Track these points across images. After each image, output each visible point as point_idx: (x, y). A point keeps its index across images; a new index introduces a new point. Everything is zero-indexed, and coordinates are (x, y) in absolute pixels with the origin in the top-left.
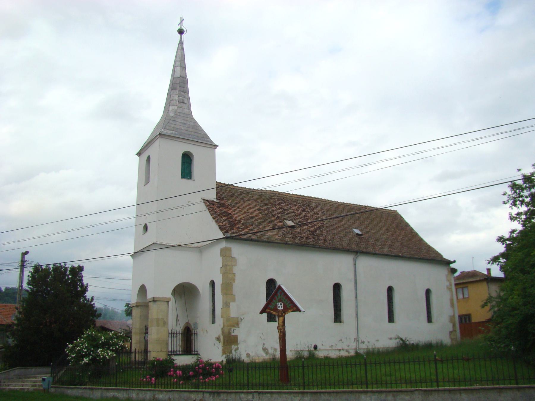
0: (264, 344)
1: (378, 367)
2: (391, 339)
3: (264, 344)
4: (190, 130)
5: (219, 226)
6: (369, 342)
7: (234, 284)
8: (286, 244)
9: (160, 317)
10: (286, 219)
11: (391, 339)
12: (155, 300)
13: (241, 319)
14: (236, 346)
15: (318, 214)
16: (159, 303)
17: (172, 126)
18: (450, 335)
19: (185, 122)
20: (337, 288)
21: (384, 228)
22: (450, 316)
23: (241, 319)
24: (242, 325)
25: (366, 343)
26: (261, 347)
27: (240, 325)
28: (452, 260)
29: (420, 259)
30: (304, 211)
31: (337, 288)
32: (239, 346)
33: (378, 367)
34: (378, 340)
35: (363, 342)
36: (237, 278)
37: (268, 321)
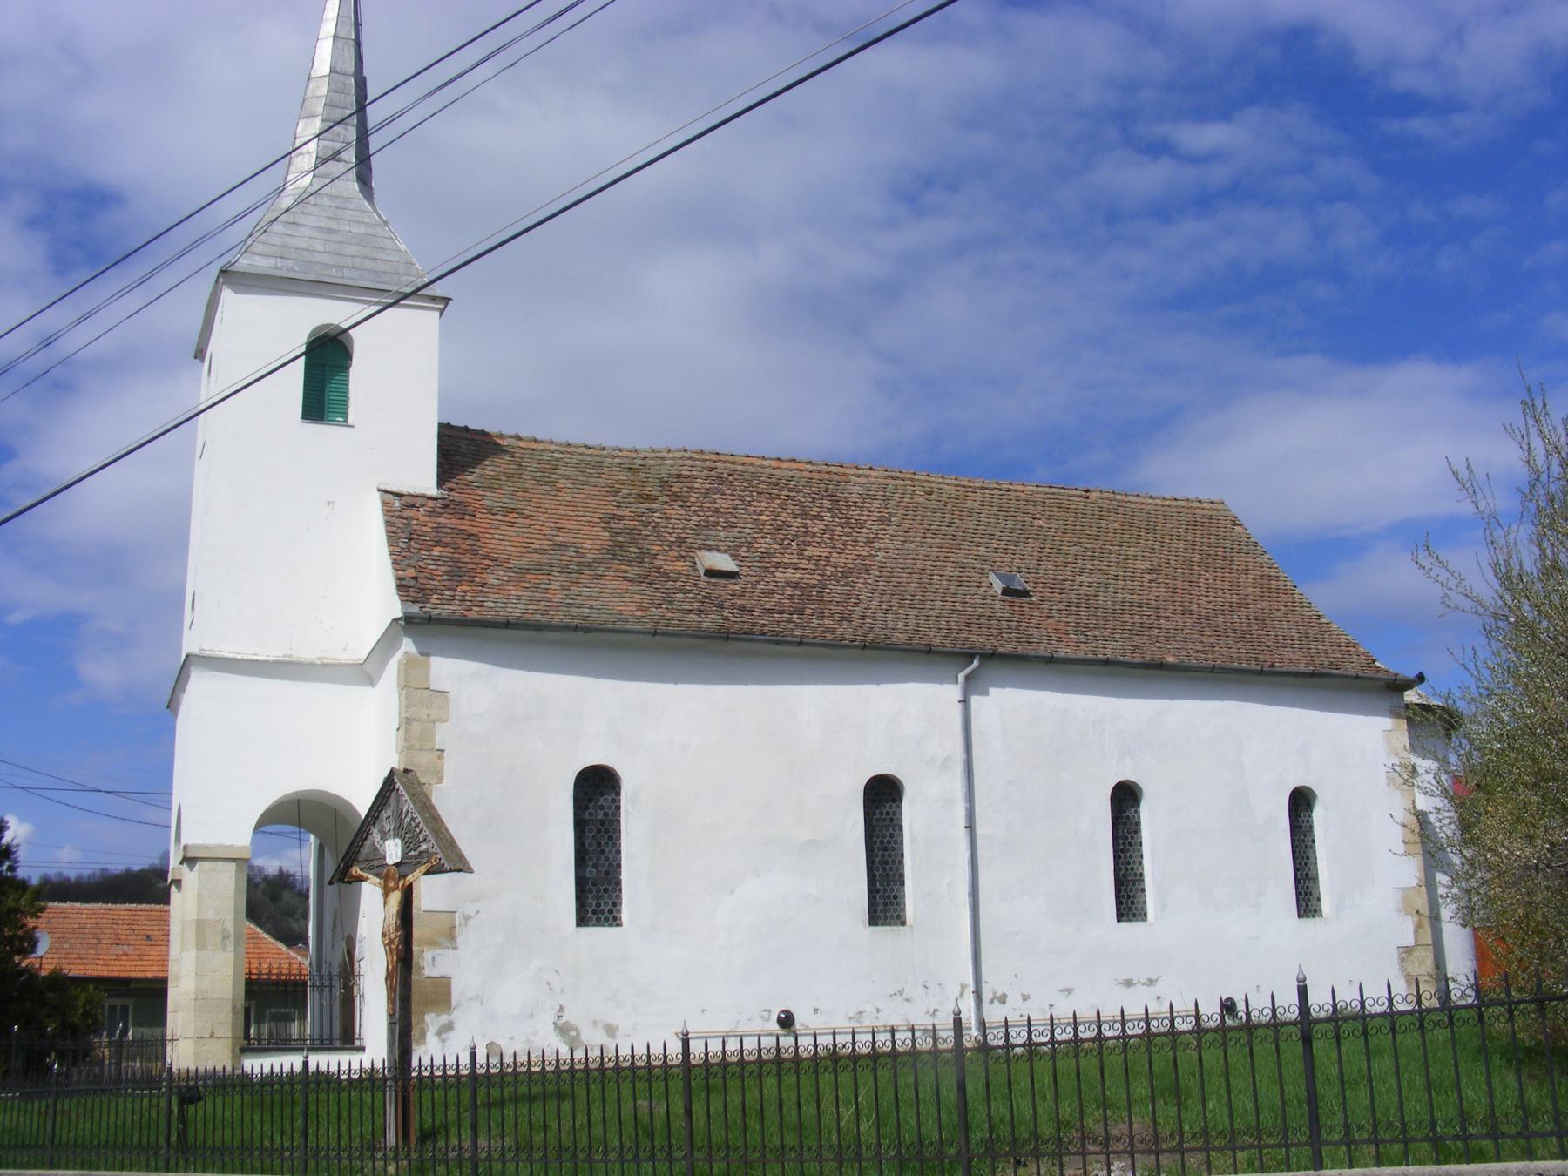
0: (562, 1009)
1: (79, 1141)
2: (1129, 983)
3: (562, 1009)
4: (349, 250)
5: (399, 579)
6: (1025, 998)
7: (435, 787)
8: (929, 652)
9: (210, 915)
10: (709, 548)
11: (1129, 983)
12: (191, 854)
13: (467, 918)
14: (444, 1019)
15: (862, 525)
16: (206, 865)
17: (278, 240)
18: (1402, 960)
19: (333, 225)
20: (882, 796)
21: (1142, 566)
22: (1405, 891)
23: (467, 918)
24: (466, 938)
25: (1014, 999)
26: (550, 1018)
27: (460, 940)
28: (1410, 673)
29: (724, 636)
30: (804, 514)
31: (882, 796)
32: (456, 1016)
33: (79, 1141)
34: (1069, 991)
35: (1003, 999)
36: (449, 765)
37: (578, 925)
